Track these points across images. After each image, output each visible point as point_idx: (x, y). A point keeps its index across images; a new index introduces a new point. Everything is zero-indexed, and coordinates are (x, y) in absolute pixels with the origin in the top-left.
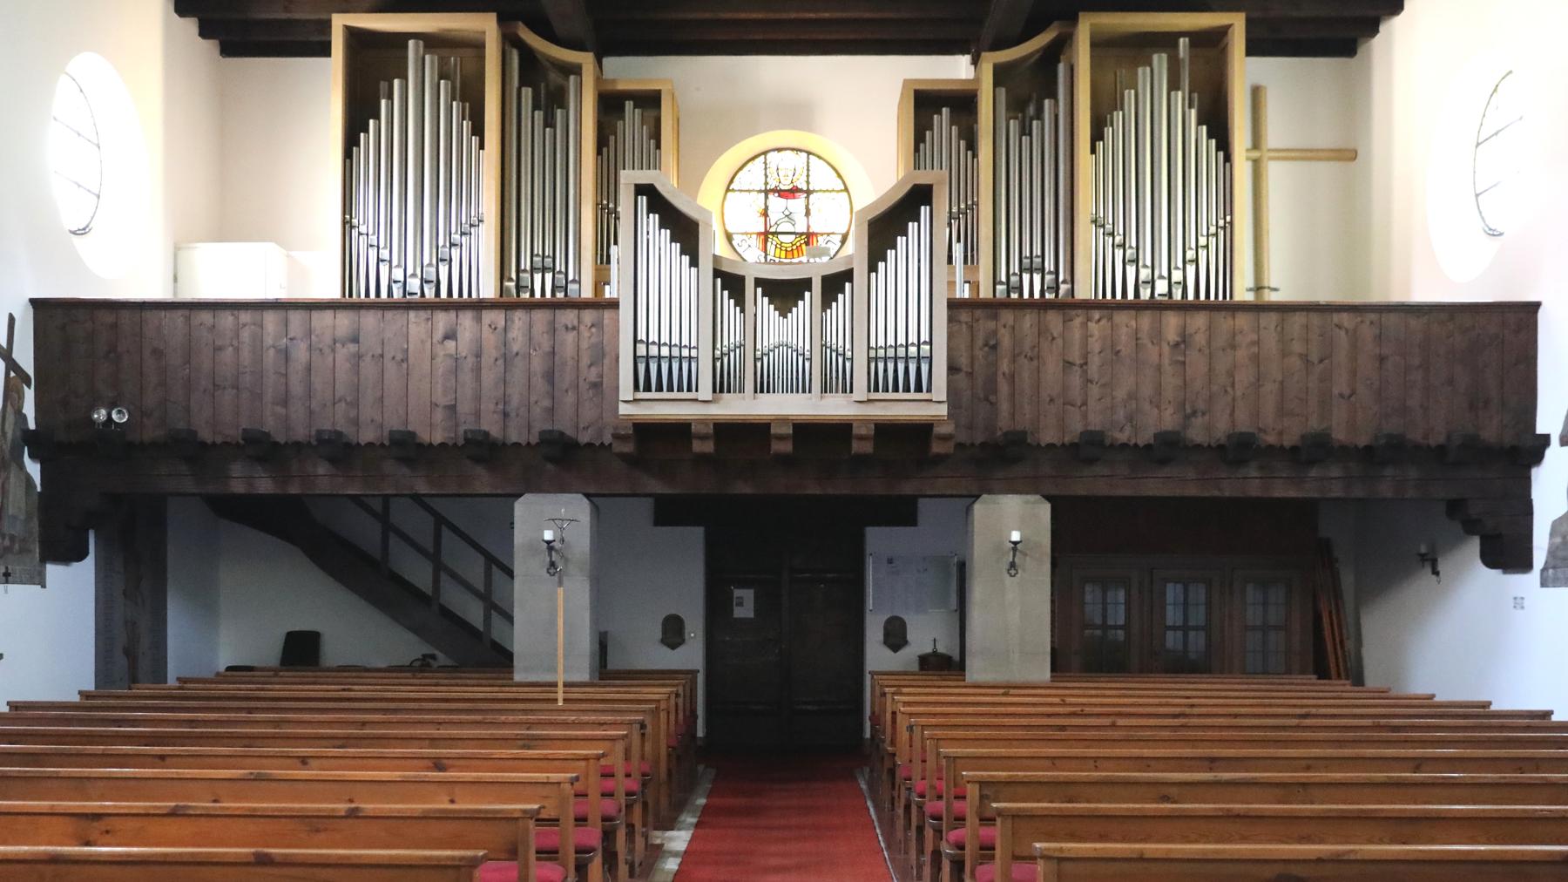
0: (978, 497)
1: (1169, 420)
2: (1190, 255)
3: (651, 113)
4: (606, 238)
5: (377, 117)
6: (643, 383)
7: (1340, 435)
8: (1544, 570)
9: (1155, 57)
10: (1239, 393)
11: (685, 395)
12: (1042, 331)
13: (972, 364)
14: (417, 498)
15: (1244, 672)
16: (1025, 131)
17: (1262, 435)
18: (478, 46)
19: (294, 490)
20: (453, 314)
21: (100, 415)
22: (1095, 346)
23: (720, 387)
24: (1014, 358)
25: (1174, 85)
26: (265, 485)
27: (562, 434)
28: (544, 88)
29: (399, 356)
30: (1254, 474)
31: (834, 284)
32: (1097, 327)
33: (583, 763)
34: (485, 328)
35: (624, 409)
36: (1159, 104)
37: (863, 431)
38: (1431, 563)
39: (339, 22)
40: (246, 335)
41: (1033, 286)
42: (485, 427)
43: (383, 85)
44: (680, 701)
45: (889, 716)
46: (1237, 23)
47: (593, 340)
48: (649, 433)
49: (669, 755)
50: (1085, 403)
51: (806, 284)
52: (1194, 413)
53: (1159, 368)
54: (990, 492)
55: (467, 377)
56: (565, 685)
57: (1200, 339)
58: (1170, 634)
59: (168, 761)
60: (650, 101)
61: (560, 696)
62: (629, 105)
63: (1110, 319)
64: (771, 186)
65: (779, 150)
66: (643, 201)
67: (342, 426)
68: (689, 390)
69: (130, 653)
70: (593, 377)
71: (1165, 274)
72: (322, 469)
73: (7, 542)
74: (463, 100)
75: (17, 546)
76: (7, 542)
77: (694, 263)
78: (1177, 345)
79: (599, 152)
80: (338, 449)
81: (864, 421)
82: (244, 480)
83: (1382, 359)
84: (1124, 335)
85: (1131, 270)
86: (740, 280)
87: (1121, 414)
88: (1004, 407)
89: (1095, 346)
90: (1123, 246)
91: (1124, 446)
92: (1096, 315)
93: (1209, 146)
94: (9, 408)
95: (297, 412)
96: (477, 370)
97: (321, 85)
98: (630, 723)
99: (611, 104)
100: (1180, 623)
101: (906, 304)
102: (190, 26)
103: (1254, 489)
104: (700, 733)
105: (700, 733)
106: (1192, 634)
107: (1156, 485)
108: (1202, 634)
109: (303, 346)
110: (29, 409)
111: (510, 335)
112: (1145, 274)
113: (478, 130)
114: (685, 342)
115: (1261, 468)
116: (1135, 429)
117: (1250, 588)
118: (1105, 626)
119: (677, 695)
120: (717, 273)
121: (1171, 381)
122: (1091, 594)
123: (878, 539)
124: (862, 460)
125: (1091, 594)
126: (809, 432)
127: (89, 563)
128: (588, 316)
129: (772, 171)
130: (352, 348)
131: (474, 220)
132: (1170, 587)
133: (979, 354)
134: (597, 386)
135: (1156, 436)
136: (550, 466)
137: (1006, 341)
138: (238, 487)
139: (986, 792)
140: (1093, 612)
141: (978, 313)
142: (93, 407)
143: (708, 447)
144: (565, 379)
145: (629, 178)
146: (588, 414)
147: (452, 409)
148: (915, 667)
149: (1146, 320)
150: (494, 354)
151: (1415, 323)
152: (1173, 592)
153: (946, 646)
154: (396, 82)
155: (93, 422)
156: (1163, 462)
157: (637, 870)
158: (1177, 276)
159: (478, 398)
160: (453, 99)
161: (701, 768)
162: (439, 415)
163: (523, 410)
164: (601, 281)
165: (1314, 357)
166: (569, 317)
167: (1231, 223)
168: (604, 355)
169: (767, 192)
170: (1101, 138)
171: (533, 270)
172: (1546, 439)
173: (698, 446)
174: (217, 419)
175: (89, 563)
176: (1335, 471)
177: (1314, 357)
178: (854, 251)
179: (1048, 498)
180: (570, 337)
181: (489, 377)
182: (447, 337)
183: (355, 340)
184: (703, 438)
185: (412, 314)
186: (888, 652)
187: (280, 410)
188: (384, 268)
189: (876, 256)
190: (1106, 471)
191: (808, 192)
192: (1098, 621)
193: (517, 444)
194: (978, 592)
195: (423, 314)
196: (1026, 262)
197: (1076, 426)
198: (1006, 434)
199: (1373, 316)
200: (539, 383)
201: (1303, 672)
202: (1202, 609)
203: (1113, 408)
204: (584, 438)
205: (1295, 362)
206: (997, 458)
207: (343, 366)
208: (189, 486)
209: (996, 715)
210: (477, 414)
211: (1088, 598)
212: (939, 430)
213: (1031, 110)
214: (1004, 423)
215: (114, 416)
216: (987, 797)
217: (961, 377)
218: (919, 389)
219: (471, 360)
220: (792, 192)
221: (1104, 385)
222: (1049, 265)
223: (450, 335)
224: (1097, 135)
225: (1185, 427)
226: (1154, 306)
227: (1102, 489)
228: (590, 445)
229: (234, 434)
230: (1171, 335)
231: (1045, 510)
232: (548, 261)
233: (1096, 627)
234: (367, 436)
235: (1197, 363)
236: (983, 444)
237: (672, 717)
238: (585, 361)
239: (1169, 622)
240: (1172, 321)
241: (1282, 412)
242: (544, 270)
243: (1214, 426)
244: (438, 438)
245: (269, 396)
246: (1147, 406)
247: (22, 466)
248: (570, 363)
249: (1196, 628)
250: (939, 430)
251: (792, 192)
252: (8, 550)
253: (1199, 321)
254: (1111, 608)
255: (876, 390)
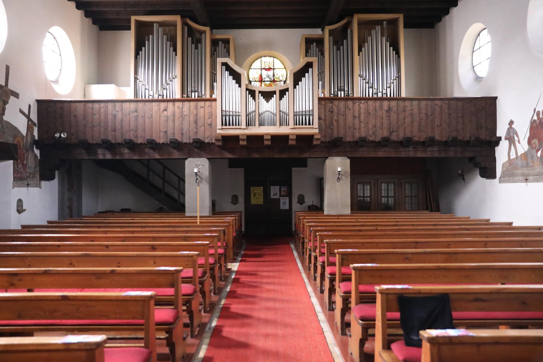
0: (327, 158)
1: (386, 134)
2: (388, 85)
3: (227, 45)
4: (213, 79)
5: (145, 46)
6: (224, 123)
7: (437, 137)
8: (500, 178)
9: (377, 27)
10: (406, 125)
11: (237, 127)
12: (346, 107)
13: (325, 117)
14: (157, 160)
15: (405, 210)
16: (338, 49)
17: (414, 138)
18: (175, 25)
19: (118, 158)
20: (166, 103)
21: (57, 135)
22: (362, 111)
23: (248, 124)
24: (338, 115)
25: (382, 36)
26: (109, 156)
27: (200, 140)
28: (195, 37)
29: (150, 116)
30: (411, 149)
31: (283, 93)
32: (363, 105)
33: (202, 247)
34: (176, 107)
35: (219, 132)
36: (378, 41)
37: (292, 137)
38: (462, 177)
39: (133, 18)
40: (102, 110)
41: (341, 94)
42: (176, 138)
43: (147, 37)
44: (237, 221)
45: (301, 226)
46: (401, 17)
47: (209, 111)
48: (226, 139)
49: (233, 239)
50: (360, 129)
51: (274, 92)
52: (393, 131)
53: (382, 118)
54: (331, 156)
55: (170, 123)
56: (200, 217)
57: (394, 109)
58: (383, 199)
59: (61, 248)
60: (226, 42)
61: (198, 221)
62: (220, 43)
63: (367, 103)
64: (263, 67)
65: (265, 56)
66: (224, 67)
67: (132, 138)
68: (239, 125)
69: (70, 208)
70: (209, 122)
71: (381, 91)
72: (126, 151)
73: (28, 175)
74: (170, 41)
75: (31, 176)
76: (28, 175)
77: (240, 86)
78: (387, 111)
79: (211, 57)
80: (131, 145)
81: (293, 134)
82: (103, 155)
83: (450, 115)
84: (371, 108)
85: (371, 90)
86: (254, 91)
87: (371, 132)
88: (335, 130)
89: (362, 111)
90: (368, 83)
91: (372, 141)
92: (363, 102)
93: (393, 53)
94: (29, 133)
95: (118, 134)
96: (174, 120)
97: (128, 39)
98: (220, 231)
99: (215, 43)
100: (386, 195)
101: (306, 98)
102: (88, 21)
103: (411, 154)
104: (243, 230)
105: (243, 230)
106: (390, 199)
107: (381, 153)
108: (393, 198)
109: (120, 113)
110: (36, 133)
111: (184, 110)
112: (375, 91)
113: (175, 50)
114: (237, 111)
115: (413, 148)
116: (375, 136)
117: (407, 185)
118: (364, 197)
119: (236, 220)
120: (247, 89)
121: (386, 122)
122: (360, 187)
123: (296, 172)
124: (292, 146)
125: (360, 187)
126: (275, 138)
127: (55, 182)
128: (208, 103)
129: (263, 63)
130: (135, 114)
131: (174, 77)
132: (383, 184)
133: (327, 114)
134: (210, 125)
135: (381, 138)
136: (196, 150)
137: (335, 110)
138: (101, 157)
139: (344, 257)
140: (360, 193)
141: (327, 101)
142: (56, 133)
143: (245, 143)
144: (200, 123)
145: (220, 60)
146: (208, 133)
147: (166, 132)
148: (307, 209)
149: (378, 103)
150: (179, 116)
151: (460, 104)
152: (384, 186)
153: (316, 203)
154: (150, 36)
155: (55, 137)
156: (385, 146)
157: (223, 278)
158: (384, 91)
159: (174, 129)
160: (168, 41)
161: (243, 241)
162: (162, 134)
163: (188, 132)
164: (212, 92)
165: (429, 114)
166: (201, 104)
167: (400, 76)
168: (212, 115)
169: (261, 69)
170: (361, 51)
171: (192, 92)
172: (500, 139)
173: (241, 143)
174: (94, 137)
175: (55, 182)
176: (436, 149)
177: (429, 114)
178: (290, 83)
179: (349, 158)
180: (202, 110)
181: (177, 123)
182: (164, 110)
183: (136, 111)
184: (243, 140)
185: (154, 103)
186: (299, 205)
187: (113, 133)
188: (147, 91)
189: (296, 83)
190: (366, 150)
191: (274, 69)
192: (362, 195)
193: (186, 143)
194: (327, 187)
195: (157, 103)
196: (339, 88)
197: (357, 136)
198: (336, 138)
199: (447, 102)
200: (193, 125)
201: (423, 210)
202: (393, 191)
203: (368, 130)
204: (207, 141)
205: (423, 115)
206: (334, 146)
207: (133, 120)
208: (86, 157)
209: (337, 226)
210: (174, 134)
211: (359, 188)
212: (316, 137)
213: (340, 43)
214: (335, 135)
215: (62, 135)
216: (344, 259)
217: (322, 121)
218: (309, 124)
219: (172, 118)
220: (269, 69)
221: (365, 123)
222: (346, 89)
223: (165, 110)
224: (360, 50)
225: (391, 135)
226: (382, 99)
227: (366, 155)
228: (208, 143)
229: (98, 141)
230: (386, 107)
231: (348, 161)
232: (196, 89)
233: (361, 197)
234: (140, 141)
235: (393, 116)
236: (329, 142)
237: (234, 227)
238: (207, 117)
239: (383, 195)
240: (386, 104)
241: (420, 131)
242: (195, 92)
243: (400, 135)
244: (161, 141)
245: (109, 129)
246: (379, 130)
247: (33, 151)
248: (202, 118)
249: (391, 197)
250: (316, 137)
251: (269, 69)
252: (28, 177)
253: (394, 103)
254: (366, 191)
255: (296, 125)
